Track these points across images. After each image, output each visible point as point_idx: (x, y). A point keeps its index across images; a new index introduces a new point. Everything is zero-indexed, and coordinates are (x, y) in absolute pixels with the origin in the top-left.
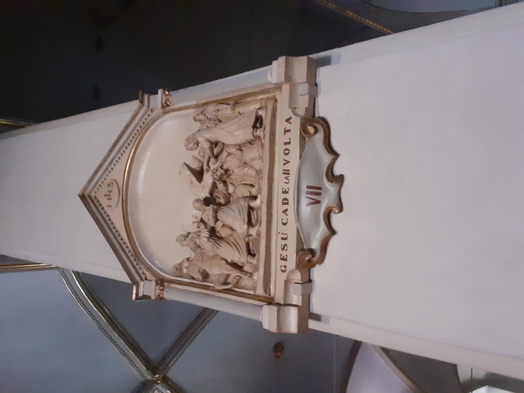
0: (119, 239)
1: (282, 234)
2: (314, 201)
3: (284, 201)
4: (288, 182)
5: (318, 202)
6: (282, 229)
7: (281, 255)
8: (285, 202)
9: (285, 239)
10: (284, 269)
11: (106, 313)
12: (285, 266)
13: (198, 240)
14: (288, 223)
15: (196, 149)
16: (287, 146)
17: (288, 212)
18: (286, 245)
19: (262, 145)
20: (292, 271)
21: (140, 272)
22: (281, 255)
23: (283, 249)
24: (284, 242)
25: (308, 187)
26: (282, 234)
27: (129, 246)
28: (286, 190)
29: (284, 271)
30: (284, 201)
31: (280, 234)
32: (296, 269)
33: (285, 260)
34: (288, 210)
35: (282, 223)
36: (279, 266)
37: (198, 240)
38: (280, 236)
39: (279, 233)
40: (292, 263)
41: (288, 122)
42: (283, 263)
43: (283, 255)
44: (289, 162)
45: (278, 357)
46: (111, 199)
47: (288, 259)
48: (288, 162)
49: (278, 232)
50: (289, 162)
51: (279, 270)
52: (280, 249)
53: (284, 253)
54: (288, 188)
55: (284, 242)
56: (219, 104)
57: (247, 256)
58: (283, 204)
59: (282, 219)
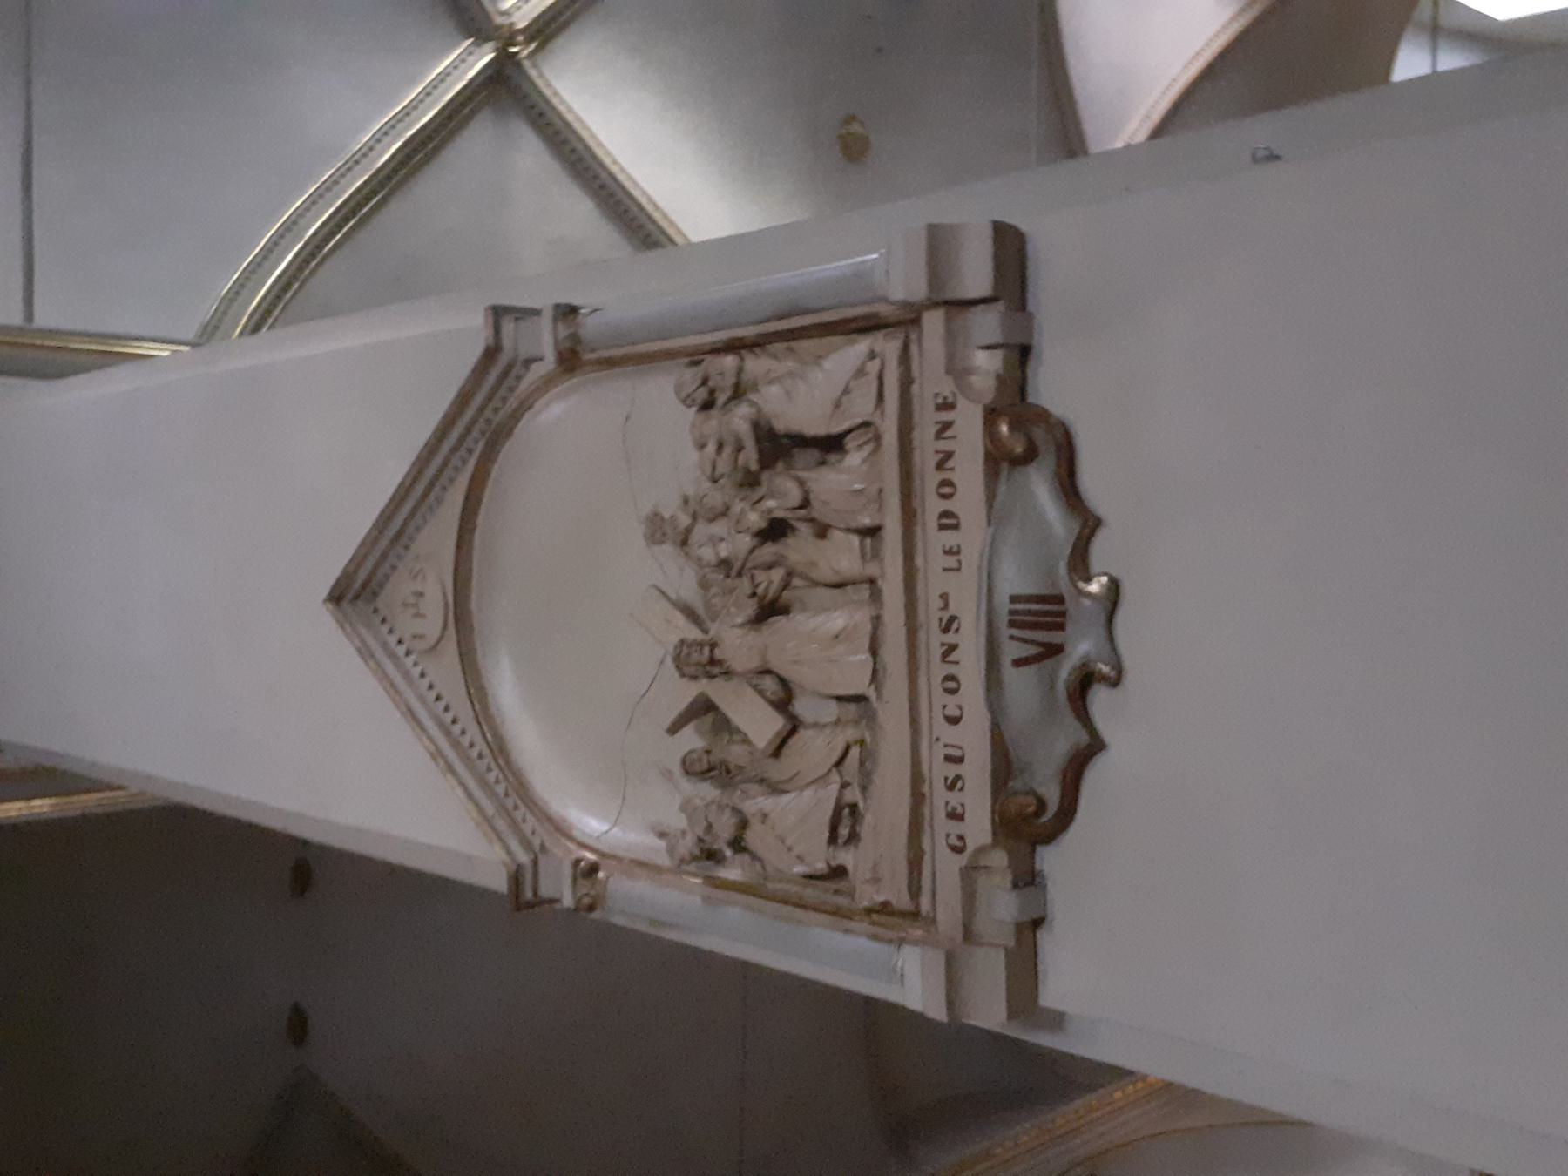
2: (1041, 649)
3: (945, 521)
4: (955, 565)
5: (1053, 651)
6: (949, 734)
8: (947, 489)
9: (960, 760)
10: (959, 844)
11: (326, 241)
12: (961, 838)
14: (964, 715)
15: (694, 678)
16: (946, 416)
18: (958, 777)
19: (878, 438)
20: (981, 851)
21: (469, 443)
22: (947, 803)
25: (1014, 599)
26: (946, 746)
28: (945, 398)
29: (958, 850)
30: (945, 521)
31: (941, 744)
32: (996, 843)
33: (961, 818)
35: (947, 843)
36: (937, 709)
38: (940, 752)
39: (938, 739)
40: (979, 827)
42: (955, 828)
46: (422, 616)
47: (967, 816)
49: (934, 738)
53: (954, 799)
54: (962, 805)
55: (952, 770)
57: (828, 848)
58: (942, 527)
59: (945, 707)
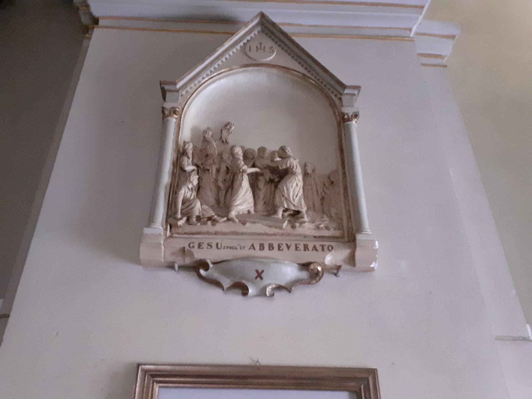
0: (335, 91)
1: (221, 243)
7: (299, 244)
13: (176, 117)
17: (253, 250)
18: (211, 247)
22: (203, 243)
23: (208, 244)
24: (214, 245)
26: (221, 243)
27: (333, 97)
31: (222, 242)
34: (317, 252)
36: (193, 240)
37: (176, 117)
41: (313, 248)
42: (196, 246)
43: (282, 246)
44: (288, 250)
45: (203, 248)
48: (253, 245)
50: (288, 250)
51: (190, 241)
52: (208, 242)
56: (259, 188)
